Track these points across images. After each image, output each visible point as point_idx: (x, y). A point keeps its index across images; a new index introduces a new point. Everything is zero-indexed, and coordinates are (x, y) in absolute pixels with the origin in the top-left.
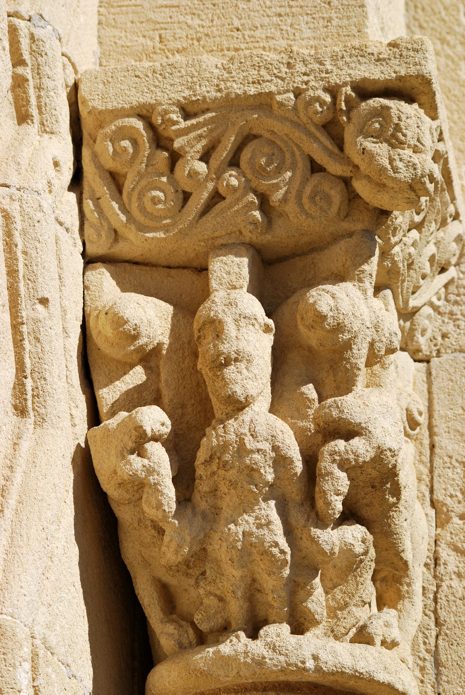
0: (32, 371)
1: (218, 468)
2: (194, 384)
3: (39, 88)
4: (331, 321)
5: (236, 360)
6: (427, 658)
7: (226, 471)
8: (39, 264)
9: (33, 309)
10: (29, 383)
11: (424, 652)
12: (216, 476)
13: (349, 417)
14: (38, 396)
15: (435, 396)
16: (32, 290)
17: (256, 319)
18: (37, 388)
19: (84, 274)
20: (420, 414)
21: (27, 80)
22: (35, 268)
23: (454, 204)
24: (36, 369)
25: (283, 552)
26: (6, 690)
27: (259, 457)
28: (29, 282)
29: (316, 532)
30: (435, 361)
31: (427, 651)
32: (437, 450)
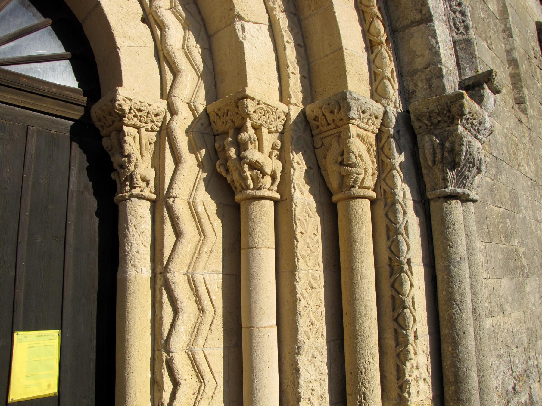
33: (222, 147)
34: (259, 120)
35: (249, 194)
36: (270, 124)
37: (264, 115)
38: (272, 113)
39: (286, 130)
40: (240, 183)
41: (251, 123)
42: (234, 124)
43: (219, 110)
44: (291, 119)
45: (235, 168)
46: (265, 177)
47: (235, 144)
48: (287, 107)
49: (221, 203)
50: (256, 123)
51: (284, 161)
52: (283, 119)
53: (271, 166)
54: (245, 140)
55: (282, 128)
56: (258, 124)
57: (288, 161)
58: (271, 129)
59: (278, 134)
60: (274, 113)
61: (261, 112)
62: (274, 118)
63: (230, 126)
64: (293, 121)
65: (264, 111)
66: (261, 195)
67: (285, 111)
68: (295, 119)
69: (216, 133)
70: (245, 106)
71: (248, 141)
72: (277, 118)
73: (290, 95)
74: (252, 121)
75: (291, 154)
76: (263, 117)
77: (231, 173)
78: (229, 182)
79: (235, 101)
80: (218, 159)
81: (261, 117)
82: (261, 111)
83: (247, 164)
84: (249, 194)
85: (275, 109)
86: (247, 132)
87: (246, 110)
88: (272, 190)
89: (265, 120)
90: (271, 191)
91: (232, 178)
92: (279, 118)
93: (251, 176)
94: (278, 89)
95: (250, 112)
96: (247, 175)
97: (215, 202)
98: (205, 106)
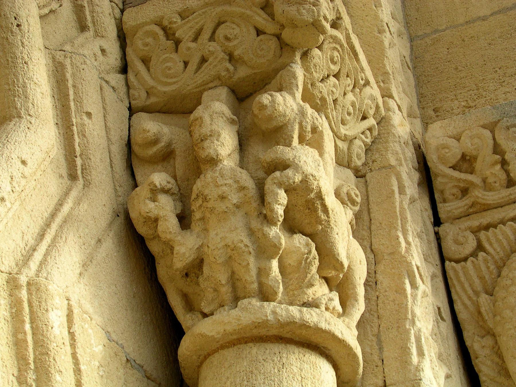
0: (80, 155)
1: (203, 202)
2: (196, 168)
3: (92, 12)
4: (271, 109)
5: (211, 135)
6: (373, 339)
7: (207, 202)
8: (84, 92)
9: (81, 119)
10: (79, 162)
11: (371, 336)
12: (202, 208)
13: (281, 156)
14: (86, 169)
15: (370, 193)
16: (80, 107)
17: (223, 114)
18: (85, 164)
19: (130, 119)
20: (357, 196)
21: (85, 7)
22: (81, 94)
23: (364, 73)
24: (84, 153)
25: (246, 246)
26: (40, 326)
27: (227, 189)
28: (78, 103)
29: (266, 229)
30: (369, 176)
31: (373, 335)
32: (372, 222)
60: (357, 90)
61: (336, 59)
76: (332, 79)
89: (336, 95)
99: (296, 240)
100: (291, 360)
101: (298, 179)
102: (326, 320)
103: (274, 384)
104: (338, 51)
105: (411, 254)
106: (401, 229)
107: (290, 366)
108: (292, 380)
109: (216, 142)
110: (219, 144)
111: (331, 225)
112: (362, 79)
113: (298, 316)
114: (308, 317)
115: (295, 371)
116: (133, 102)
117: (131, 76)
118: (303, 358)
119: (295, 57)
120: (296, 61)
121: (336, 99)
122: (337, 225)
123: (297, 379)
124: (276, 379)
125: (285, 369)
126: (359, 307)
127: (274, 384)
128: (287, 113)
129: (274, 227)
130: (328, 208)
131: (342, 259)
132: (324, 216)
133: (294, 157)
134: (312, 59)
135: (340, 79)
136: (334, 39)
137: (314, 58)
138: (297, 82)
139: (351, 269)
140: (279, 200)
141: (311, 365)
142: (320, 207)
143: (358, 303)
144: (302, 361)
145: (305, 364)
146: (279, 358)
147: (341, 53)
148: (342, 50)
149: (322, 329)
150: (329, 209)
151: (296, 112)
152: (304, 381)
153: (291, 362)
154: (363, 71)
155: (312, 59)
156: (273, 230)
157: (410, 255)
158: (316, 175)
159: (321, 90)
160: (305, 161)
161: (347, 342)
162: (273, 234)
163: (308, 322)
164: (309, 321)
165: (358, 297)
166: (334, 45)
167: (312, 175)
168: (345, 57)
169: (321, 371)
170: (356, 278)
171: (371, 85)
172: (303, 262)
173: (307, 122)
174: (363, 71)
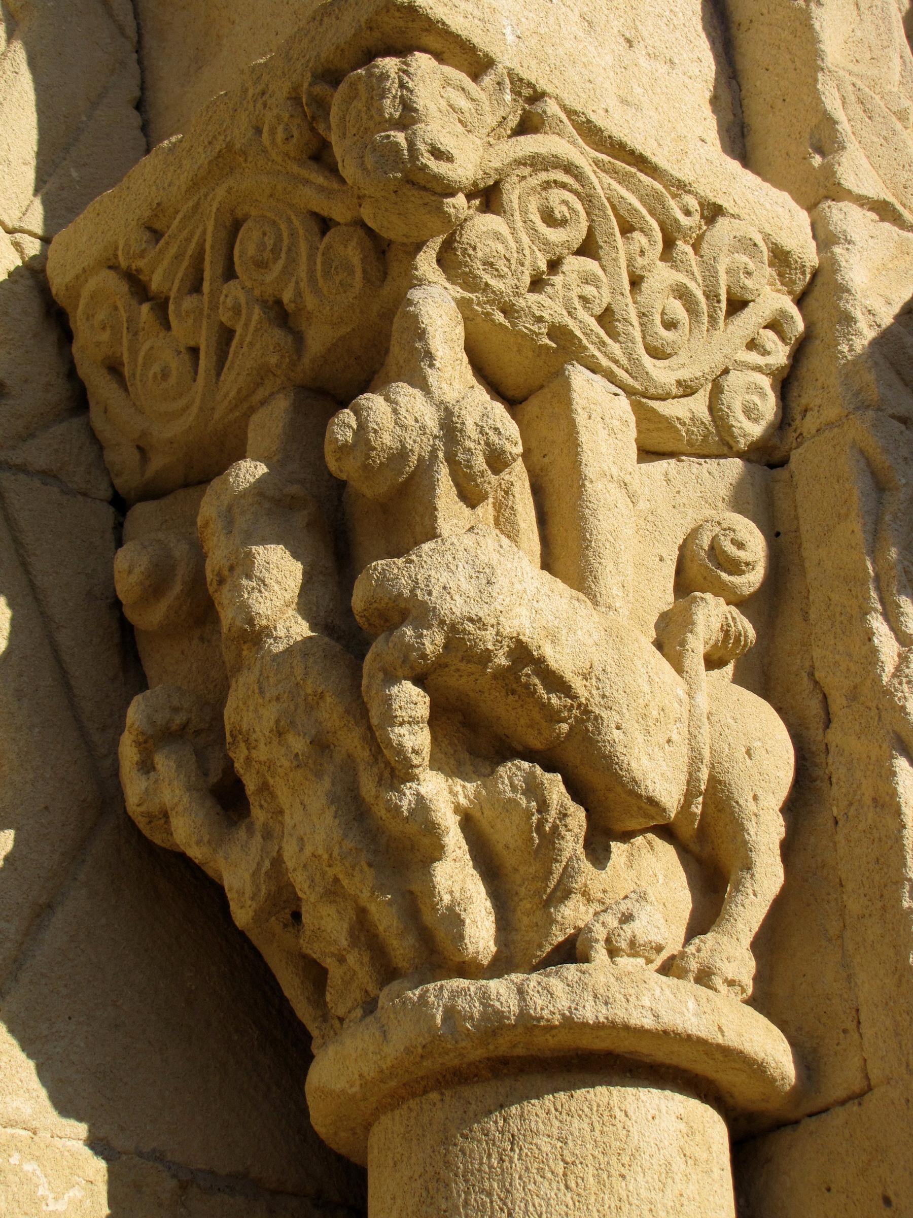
33: (177, 588)
34: (537, 284)
35: (450, 1013)
36: (656, 353)
37: (588, 248)
38: (669, 244)
39: (809, 424)
40: (362, 913)
41: (463, 305)
42: (299, 339)
43: (156, 234)
44: (848, 319)
45: (298, 744)
46: (618, 849)
47: (300, 518)
48: (803, 218)
49: (158, 1157)
50: (508, 310)
51: (814, 706)
52: (774, 325)
53: (678, 733)
54: (402, 454)
55: (769, 406)
56: (526, 325)
57: (853, 695)
58: (665, 408)
59: (734, 467)
60: (683, 247)
61: (560, 211)
62: (682, 293)
63: (262, 374)
64: (876, 343)
65: (588, 200)
66: (590, 1012)
67: (789, 243)
68: (887, 318)
69: (127, 482)
70: (390, 108)
71: (426, 468)
72: (712, 296)
73: (832, 122)
74: (470, 282)
75: (878, 624)
76: (574, 264)
77: (259, 815)
78: (242, 915)
79: (295, 99)
80: (142, 684)
81: (554, 265)
82: (556, 196)
83: (419, 681)
84: (450, 1013)
85: (692, 203)
86: (424, 387)
87: (400, 137)
88: (704, 977)
89: (603, 298)
90: (688, 986)
91: (278, 862)
92: (737, 305)
93: (468, 823)
94: (715, 101)
95: (438, 154)
96: (422, 805)
97: (97, 1144)
98: (33, 247)
99: (503, 783)
100: (533, 1118)
101: (432, 643)
102: (595, 996)
103: (491, 1202)
104: (564, 186)
105: (907, 676)
106: (879, 607)
107: (529, 1139)
108: (539, 1179)
109: (244, 582)
110: (254, 584)
111: (592, 712)
112: (688, 213)
113: (515, 1009)
114: (540, 1002)
115: (546, 1148)
116: (117, 482)
117: (95, 412)
118: (566, 1106)
119: (416, 269)
120: (421, 280)
121: (608, 310)
122: (610, 703)
123: (553, 1173)
124: (495, 1185)
125: (517, 1151)
126: (756, 888)
127: (491, 1202)
128: (409, 444)
129: (408, 784)
130: (562, 677)
131: (651, 789)
132: (560, 698)
133: (412, 584)
134: (471, 252)
135: (601, 253)
136: (531, 165)
137: (474, 249)
138: (427, 344)
139: (720, 782)
140: (398, 713)
141: (595, 1118)
142: (537, 681)
143: (753, 875)
144: (564, 1116)
145: (576, 1121)
146: (501, 1123)
147: (576, 186)
148: (576, 177)
149: (585, 1025)
150: (569, 676)
151: (436, 431)
152: (573, 1172)
153: (533, 1125)
154: (688, 188)
155: (471, 252)
156: (407, 792)
157: (904, 680)
158: (481, 614)
159: (538, 313)
160: (445, 588)
161: (680, 1030)
162: (410, 804)
163: (542, 1018)
164: (545, 1013)
165: (753, 855)
166: (544, 176)
167: (471, 620)
168: (592, 191)
169: (629, 1123)
170: (741, 802)
171: (731, 211)
172: (535, 835)
173: (469, 450)
174: (688, 188)
